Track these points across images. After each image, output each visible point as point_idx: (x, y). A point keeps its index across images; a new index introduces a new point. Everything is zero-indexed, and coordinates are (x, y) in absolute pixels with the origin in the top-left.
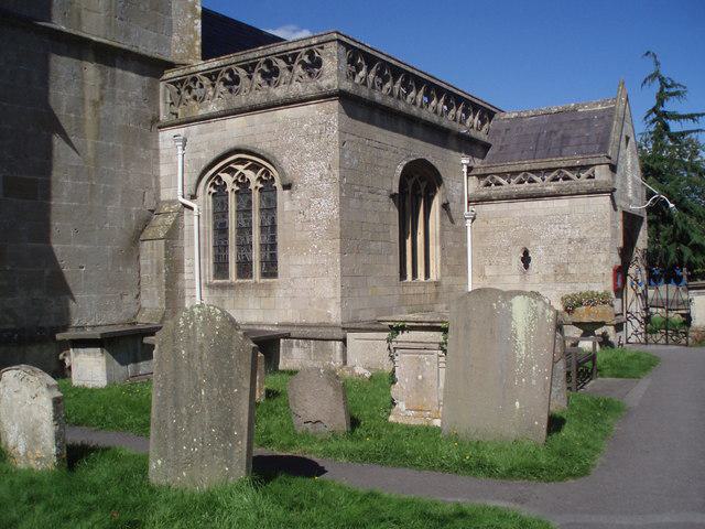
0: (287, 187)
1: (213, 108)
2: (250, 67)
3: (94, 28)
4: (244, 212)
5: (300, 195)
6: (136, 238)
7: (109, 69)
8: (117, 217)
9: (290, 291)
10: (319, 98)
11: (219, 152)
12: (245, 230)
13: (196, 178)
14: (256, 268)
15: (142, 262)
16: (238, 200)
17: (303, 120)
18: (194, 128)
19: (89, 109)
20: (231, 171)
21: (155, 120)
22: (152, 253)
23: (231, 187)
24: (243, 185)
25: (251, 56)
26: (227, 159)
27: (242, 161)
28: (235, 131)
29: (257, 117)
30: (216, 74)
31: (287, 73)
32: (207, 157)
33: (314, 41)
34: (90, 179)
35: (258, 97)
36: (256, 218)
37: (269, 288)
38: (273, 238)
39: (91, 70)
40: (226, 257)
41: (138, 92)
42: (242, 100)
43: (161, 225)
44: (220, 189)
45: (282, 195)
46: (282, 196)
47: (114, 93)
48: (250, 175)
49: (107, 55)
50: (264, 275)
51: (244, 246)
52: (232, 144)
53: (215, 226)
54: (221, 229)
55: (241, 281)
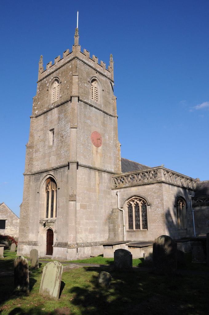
9: (151, 233)
10: (157, 183)
11: (130, 196)
17: (153, 188)
20: (134, 201)
23: (133, 205)
24: (137, 205)
27: (136, 199)
28: (134, 191)
29: (140, 188)
30: (128, 176)
32: (126, 197)
33: (155, 169)
42: (135, 183)
46: (148, 207)
47: (102, 181)
51: (138, 220)
53: (128, 215)
54: (130, 216)
55: (137, 230)
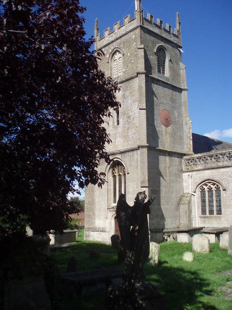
0: (224, 190)
1: (200, 167)
2: (211, 156)
3: (168, 148)
4: (211, 196)
5: (228, 192)
6: (179, 204)
7: (171, 158)
8: (174, 199)
11: (203, 180)
12: (211, 201)
13: (196, 186)
14: (215, 212)
15: (181, 210)
16: (208, 193)
18: (194, 173)
19: (167, 169)
20: (206, 185)
21: (182, 170)
22: (183, 208)
24: (210, 189)
25: (211, 154)
26: (205, 182)
27: (210, 183)
28: (207, 174)
29: (214, 171)
31: (222, 159)
34: (168, 188)
35: (214, 165)
36: (214, 198)
37: (220, 218)
38: (220, 204)
39: (167, 158)
40: (205, 209)
41: (178, 163)
42: (209, 166)
43: (186, 200)
44: (203, 190)
45: (222, 192)
48: (212, 186)
49: (171, 154)
50: (217, 214)
51: (211, 206)
52: (207, 178)
54: (203, 201)
